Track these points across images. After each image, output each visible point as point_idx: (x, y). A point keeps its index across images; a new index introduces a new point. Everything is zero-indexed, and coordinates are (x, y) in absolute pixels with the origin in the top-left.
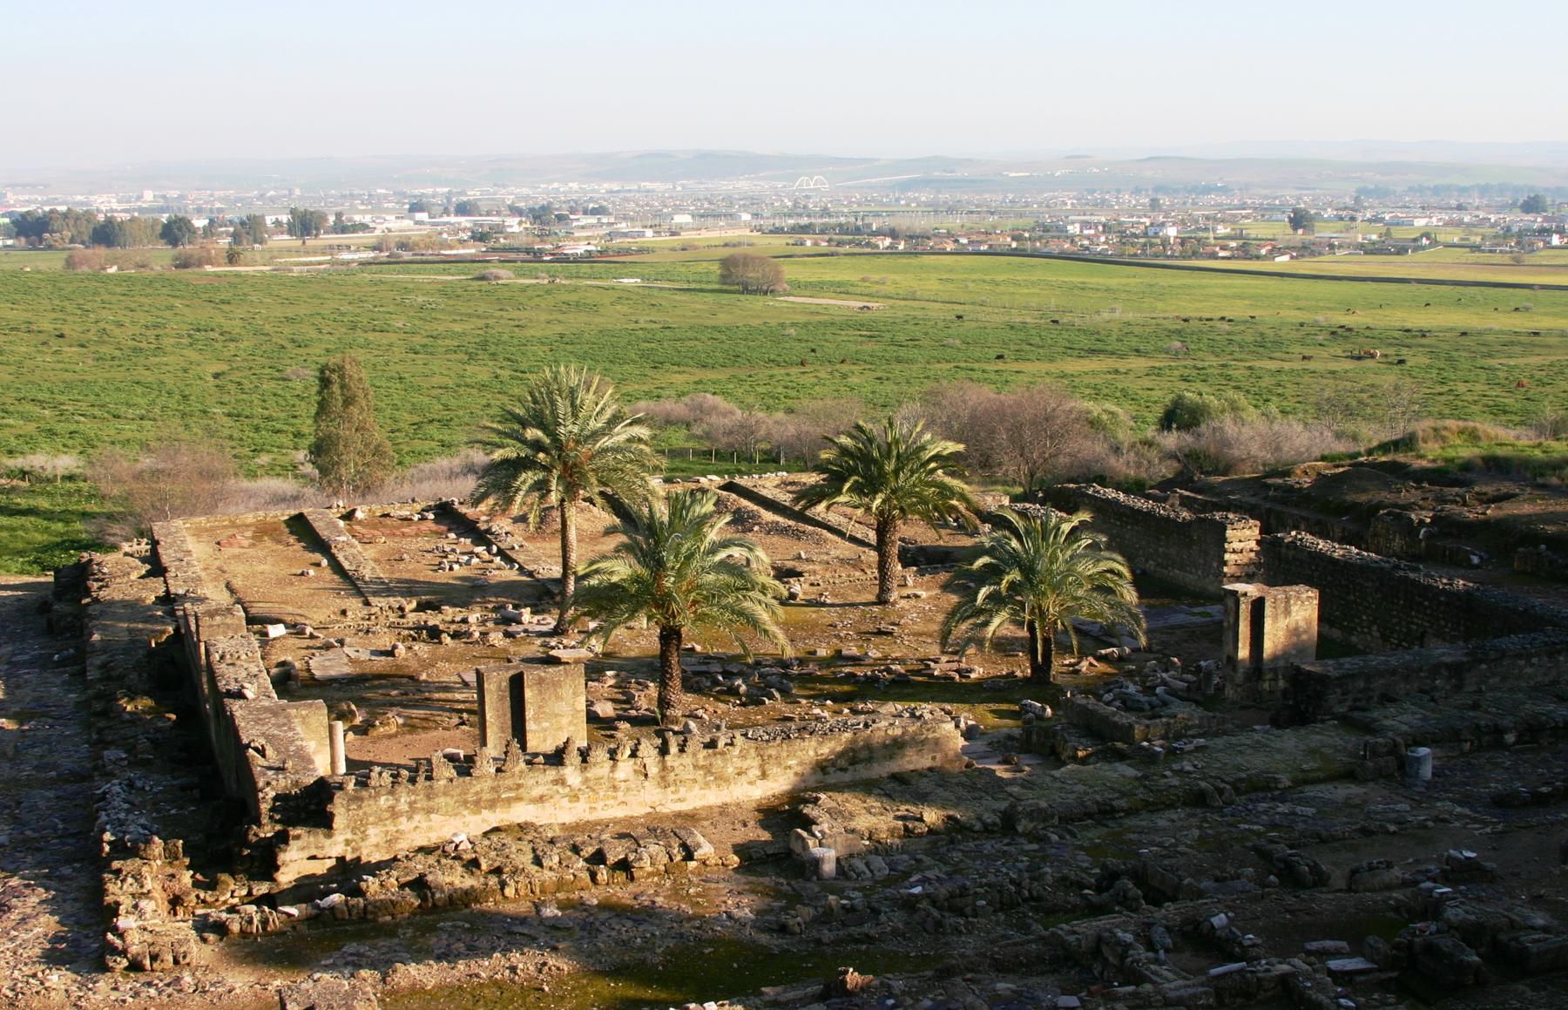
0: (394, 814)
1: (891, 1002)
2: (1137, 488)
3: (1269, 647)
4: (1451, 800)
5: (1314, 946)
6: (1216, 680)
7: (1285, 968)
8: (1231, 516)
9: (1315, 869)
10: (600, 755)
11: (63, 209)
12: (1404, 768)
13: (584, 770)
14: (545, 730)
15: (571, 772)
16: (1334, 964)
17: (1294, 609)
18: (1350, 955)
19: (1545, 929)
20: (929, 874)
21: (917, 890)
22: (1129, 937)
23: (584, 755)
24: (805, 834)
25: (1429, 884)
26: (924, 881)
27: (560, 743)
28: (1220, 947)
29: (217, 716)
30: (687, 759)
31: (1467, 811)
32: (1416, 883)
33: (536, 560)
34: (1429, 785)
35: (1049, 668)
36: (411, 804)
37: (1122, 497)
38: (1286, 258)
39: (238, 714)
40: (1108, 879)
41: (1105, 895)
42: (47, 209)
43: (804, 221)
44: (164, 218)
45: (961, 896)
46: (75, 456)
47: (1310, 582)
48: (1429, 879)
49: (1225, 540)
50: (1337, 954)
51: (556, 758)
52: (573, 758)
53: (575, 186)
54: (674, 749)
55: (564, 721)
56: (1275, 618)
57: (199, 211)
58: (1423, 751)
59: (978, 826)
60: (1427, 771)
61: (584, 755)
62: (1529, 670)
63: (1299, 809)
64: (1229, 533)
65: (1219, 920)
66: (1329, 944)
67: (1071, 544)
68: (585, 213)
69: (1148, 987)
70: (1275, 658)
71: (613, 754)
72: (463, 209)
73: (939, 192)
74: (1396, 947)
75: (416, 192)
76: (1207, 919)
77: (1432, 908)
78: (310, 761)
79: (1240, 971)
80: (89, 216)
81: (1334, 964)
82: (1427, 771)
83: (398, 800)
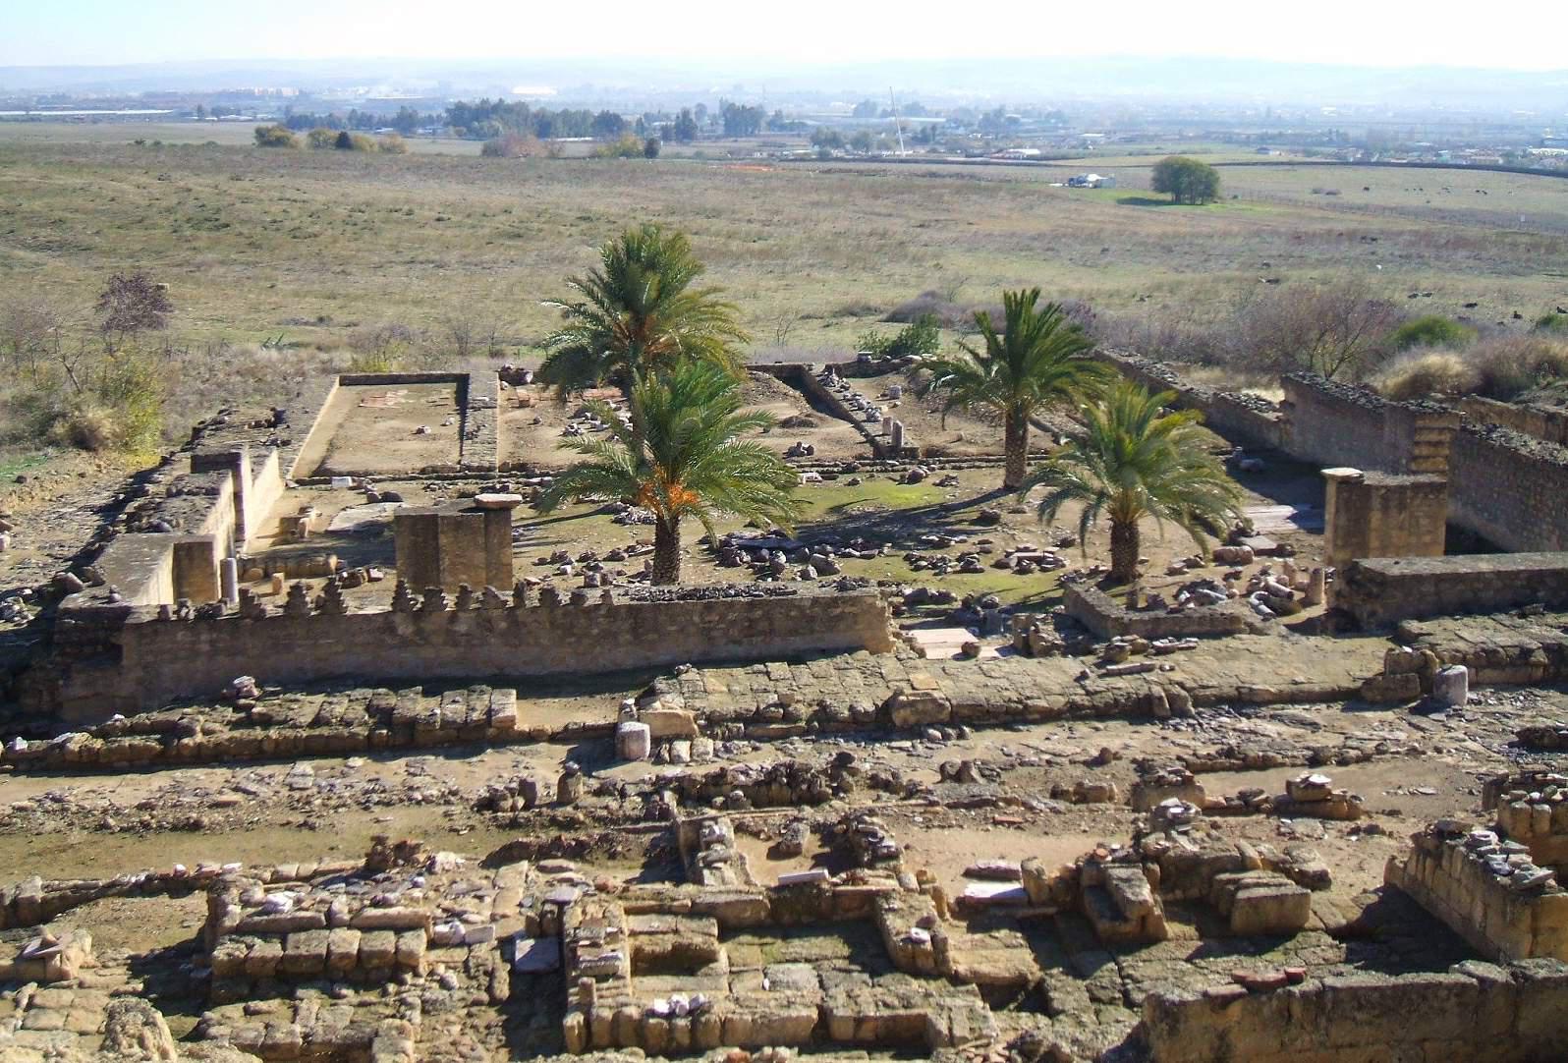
36: (212, 642)
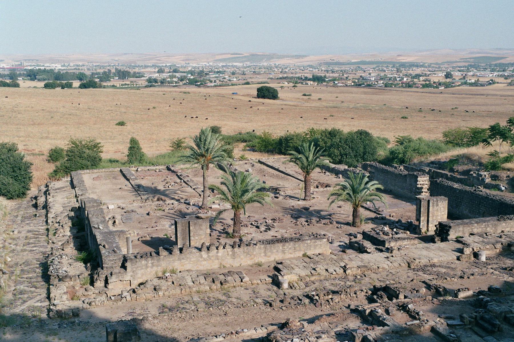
0: (147, 267)
8: (419, 173)
10: (213, 248)
11: (43, 68)
13: (208, 253)
14: (197, 239)
15: (204, 254)
17: (440, 204)
23: (208, 249)
24: (278, 274)
29: (91, 235)
30: (241, 249)
35: (247, 56)
36: (152, 263)
37: (384, 166)
38: (443, 88)
42: (37, 68)
43: (285, 75)
46: (103, 158)
49: (417, 181)
53: (211, 64)
55: (203, 237)
56: (433, 206)
61: (208, 249)
64: (419, 179)
67: (25, 291)
73: (329, 67)
76: (407, 306)
83: (148, 262)
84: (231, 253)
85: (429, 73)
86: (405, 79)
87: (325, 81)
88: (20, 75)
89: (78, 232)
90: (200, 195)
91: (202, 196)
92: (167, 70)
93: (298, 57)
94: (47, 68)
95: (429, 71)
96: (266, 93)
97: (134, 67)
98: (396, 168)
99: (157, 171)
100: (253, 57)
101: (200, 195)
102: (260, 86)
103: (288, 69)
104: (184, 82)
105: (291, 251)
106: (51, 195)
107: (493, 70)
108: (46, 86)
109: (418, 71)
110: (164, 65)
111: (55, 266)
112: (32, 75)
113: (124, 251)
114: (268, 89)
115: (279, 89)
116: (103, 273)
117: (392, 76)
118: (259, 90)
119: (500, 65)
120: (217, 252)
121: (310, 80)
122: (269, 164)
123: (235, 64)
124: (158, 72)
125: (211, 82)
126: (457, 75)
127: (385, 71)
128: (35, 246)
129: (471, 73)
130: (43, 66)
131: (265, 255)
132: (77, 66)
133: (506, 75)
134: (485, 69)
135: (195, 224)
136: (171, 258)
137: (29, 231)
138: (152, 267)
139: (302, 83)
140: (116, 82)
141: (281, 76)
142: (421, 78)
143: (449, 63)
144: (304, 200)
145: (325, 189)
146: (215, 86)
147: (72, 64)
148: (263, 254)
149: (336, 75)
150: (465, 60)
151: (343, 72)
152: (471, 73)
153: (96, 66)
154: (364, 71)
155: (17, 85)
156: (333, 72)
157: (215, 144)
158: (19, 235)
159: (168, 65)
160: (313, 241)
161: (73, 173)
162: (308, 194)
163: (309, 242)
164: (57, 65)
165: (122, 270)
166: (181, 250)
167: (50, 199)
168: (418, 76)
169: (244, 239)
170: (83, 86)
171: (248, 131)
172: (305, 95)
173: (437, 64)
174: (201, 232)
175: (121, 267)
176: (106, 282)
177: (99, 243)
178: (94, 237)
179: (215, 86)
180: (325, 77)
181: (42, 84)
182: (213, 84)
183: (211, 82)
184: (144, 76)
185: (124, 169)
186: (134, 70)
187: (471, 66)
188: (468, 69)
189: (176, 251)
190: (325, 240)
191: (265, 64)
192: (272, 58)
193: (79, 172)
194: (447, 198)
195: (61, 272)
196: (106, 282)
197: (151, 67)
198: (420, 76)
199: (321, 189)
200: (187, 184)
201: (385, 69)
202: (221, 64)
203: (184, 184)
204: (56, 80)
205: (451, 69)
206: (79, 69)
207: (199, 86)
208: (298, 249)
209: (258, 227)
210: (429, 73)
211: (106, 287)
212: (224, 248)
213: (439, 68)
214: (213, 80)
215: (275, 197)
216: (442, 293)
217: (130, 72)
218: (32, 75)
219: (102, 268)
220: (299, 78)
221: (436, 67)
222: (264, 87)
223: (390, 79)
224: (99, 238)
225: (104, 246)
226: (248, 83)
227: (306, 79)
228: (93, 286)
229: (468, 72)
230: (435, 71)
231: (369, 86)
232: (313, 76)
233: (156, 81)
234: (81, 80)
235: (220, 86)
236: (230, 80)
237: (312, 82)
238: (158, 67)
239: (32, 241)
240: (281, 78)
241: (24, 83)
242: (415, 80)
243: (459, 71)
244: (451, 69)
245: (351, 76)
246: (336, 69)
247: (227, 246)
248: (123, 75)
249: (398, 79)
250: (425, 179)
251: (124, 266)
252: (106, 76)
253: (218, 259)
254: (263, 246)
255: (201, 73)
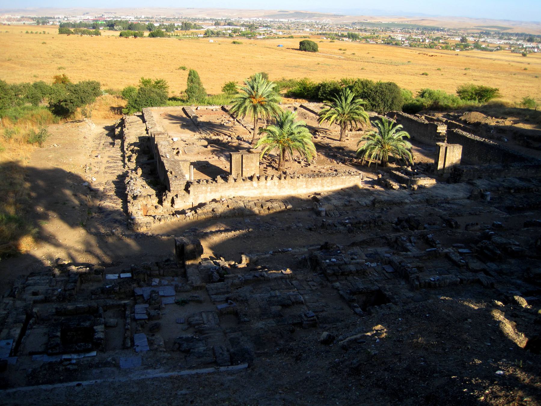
0: (206, 192)
1: (339, 252)
2: (387, 272)
3: (447, 165)
4: (495, 207)
5: (455, 245)
6: (432, 169)
7: (447, 250)
9: (456, 223)
10: (263, 179)
11: (120, 20)
12: (483, 196)
16: (460, 250)
17: (455, 151)
18: (464, 248)
19: (518, 245)
20: (350, 217)
21: (347, 221)
22: (405, 239)
23: (258, 178)
25: (487, 231)
26: (349, 219)
27: (252, 175)
28: (430, 243)
30: (286, 181)
31: (499, 210)
32: (485, 229)
33: (247, 123)
34: (489, 202)
36: (211, 189)
39: (164, 161)
40: (400, 221)
41: (399, 227)
42: (115, 19)
43: (324, 32)
44: (147, 23)
45: (359, 224)
47: (460, 143)
48: (488, 229)
50: (461, 247)
51: (251, 178)
52: (255, 179)
53: (261, 19)
54: (283, 178)
55: (253, 169)
56: (450, 154)
57: (157, 21)
58: (489, 193)
59: (365, 205)
60: (488, 199)
61: (258, 178)
62: (519, 172)
63: (453, 206)
64: (438, 128)
65: (430, 236)
66: (459, 245)
68: (263, 27)
69: (409, 253)
70: (448, 167)
71: (266, 178)
72: (229, 24)
74: (478, 247)
75: (217, 19)
77: (488, 237)
78: (184, 176)
79: (435, 251)
80: (127, 22)
81: (460, 250)
82: (488, 199)
84: (277, 184)
85: (447, 37)
86: (427, 41)
87: (358, 38)
88: (101, 25)
89: (148, 160)
90: (250, 132)
91: (252, 133)
92: (223, 22)
93: (335, 16)
94: (123, 20)
95: (448, 35)
96: (306, 46)
97: (195, 20)
98: (418, 117)
99: (214, 110)
100: (297, 14)
101: (250, 132)
102: (302, 40)
103: (327, 26)
104: (237, 34)
105: (328, 185)
106: (127, 127)
107: (501, 38)
108: (121, 35)
109: (438, 34)
110: (220, 19)
111: (131, 187)
112: (111, 26)
113: (187, 178)
114: (309, 43)
115: (319, 44)
116: (170, 195)
117: (416, 37)
118: (301, 43)
119: (507, 34)
120: (266, 183)
121: (345, 37)
122: (310, 108)
123: (281, 20)
124: (215, 25)
125: (260, 35)
126: (470, 39)
127: (410, 33)
128: (115, 170)
129: (482, 40)
130: (120, 18)
131: (307, 187)
132: (148, 18)
133: (511, 43)
134: (494, 37)
135: (247, 158)
136: (227, 185)
137: (109, 157)
138: (211, 193)
139: (339, 40)
140: (180, 32)
141: (320, 32)
142: (441, 41)
143: (465, 29)
144: (340, 140)
145: (358, 132)
146: (264, 38)
147: (143, 17)
148: (304, 186)
149: (368, 34)
150: (478, 28)
151: (374, 31)
152: (482, 40)
153: (163, 18)
154: (393, 32)
155: (97, 34)
156: (365, 31)
157: (264, 89)
158: (102, 159)
159: (223, 19)
160: (348, 177)
161: (144, 110)
162: (343, 136)
163: (344, 177)
164: (131, 17)
165: (187, 194)
166: (235, 180)
167: (125, 131)
168: (438, 39)
169: (288, 172)
170: (152, 35)
171: (291, 78)
172: (340, 50)
173: (454, 30)
174: (252, 165)
175: (184, 190)
176: (173, 202)
177: (167, 169)
178: (162, 163)
179: (264, 38)
180: (359, 35)
181: (118, 33)
182: (262, 37)
183: (260, 35)
184: (203, 28)
185: (185, 107)
186: (195, 23)
187: (482, 33)
188: (480, 35)
189: (231, 178)
190: (358, 177)
191: (308, 21)
192: (314, 16)
193: (150, 108)
194: (461, 147)
195: (136, 192)
196: (173, 202)
197: (209, 20)
198: (440, 39)
199: (354, 132)
200: (239, 122)
201: (410, 31)
202: (269, 20)
203: (237, 123)
204: (131, 29)
205: (466, 34)
206: (148, 21)
207: (250, 38)
208: (335, 183)
209: (299, 162)
210: (447, 37)
211: (172, 206)
212: (272, 179)
213: (456, 33)
214: (262, 33)
215: (315, 137)
216: (454, 226)
217: (190, 24)
218: (111, 26)
219: (170, 191)
220: (336, 35)
221: (453, 32)
222: (306, 41)
223: (414, 40)
224: (167, 166)
225: (171, 173)
226: (292, 37)
227: (343, 36)
228: (162, 205)
229: (479, 38)
230: (452, 35)
231: (396, 44)
232: (348, 33)
233: (212, 33)
234: (150, 30)
235: (267, 38)
236: (276, 34)
237: (347, 39)
238: (215, 20)
239: (111, 165)
240: (321, 34)
241: (105, 33)
242: (435, 42)
243: (473, 37)
244: (466, 34)
245: (382, 36)
246: (369, 28)
247: (275, 178)
248: (186, 26)
249: (421, 41)
250: (444, 128)
251: (187, 190)
252: (171, 28)
253: (266, 188)
254: (304, 179)
255: (251, 27)
